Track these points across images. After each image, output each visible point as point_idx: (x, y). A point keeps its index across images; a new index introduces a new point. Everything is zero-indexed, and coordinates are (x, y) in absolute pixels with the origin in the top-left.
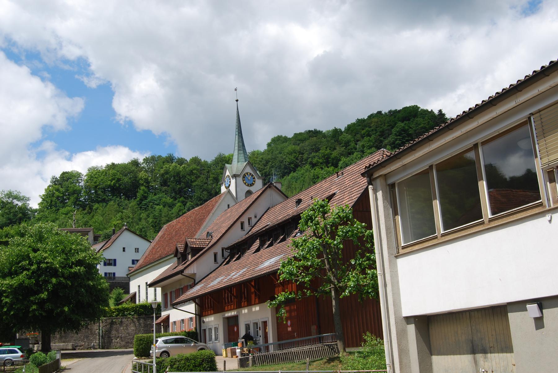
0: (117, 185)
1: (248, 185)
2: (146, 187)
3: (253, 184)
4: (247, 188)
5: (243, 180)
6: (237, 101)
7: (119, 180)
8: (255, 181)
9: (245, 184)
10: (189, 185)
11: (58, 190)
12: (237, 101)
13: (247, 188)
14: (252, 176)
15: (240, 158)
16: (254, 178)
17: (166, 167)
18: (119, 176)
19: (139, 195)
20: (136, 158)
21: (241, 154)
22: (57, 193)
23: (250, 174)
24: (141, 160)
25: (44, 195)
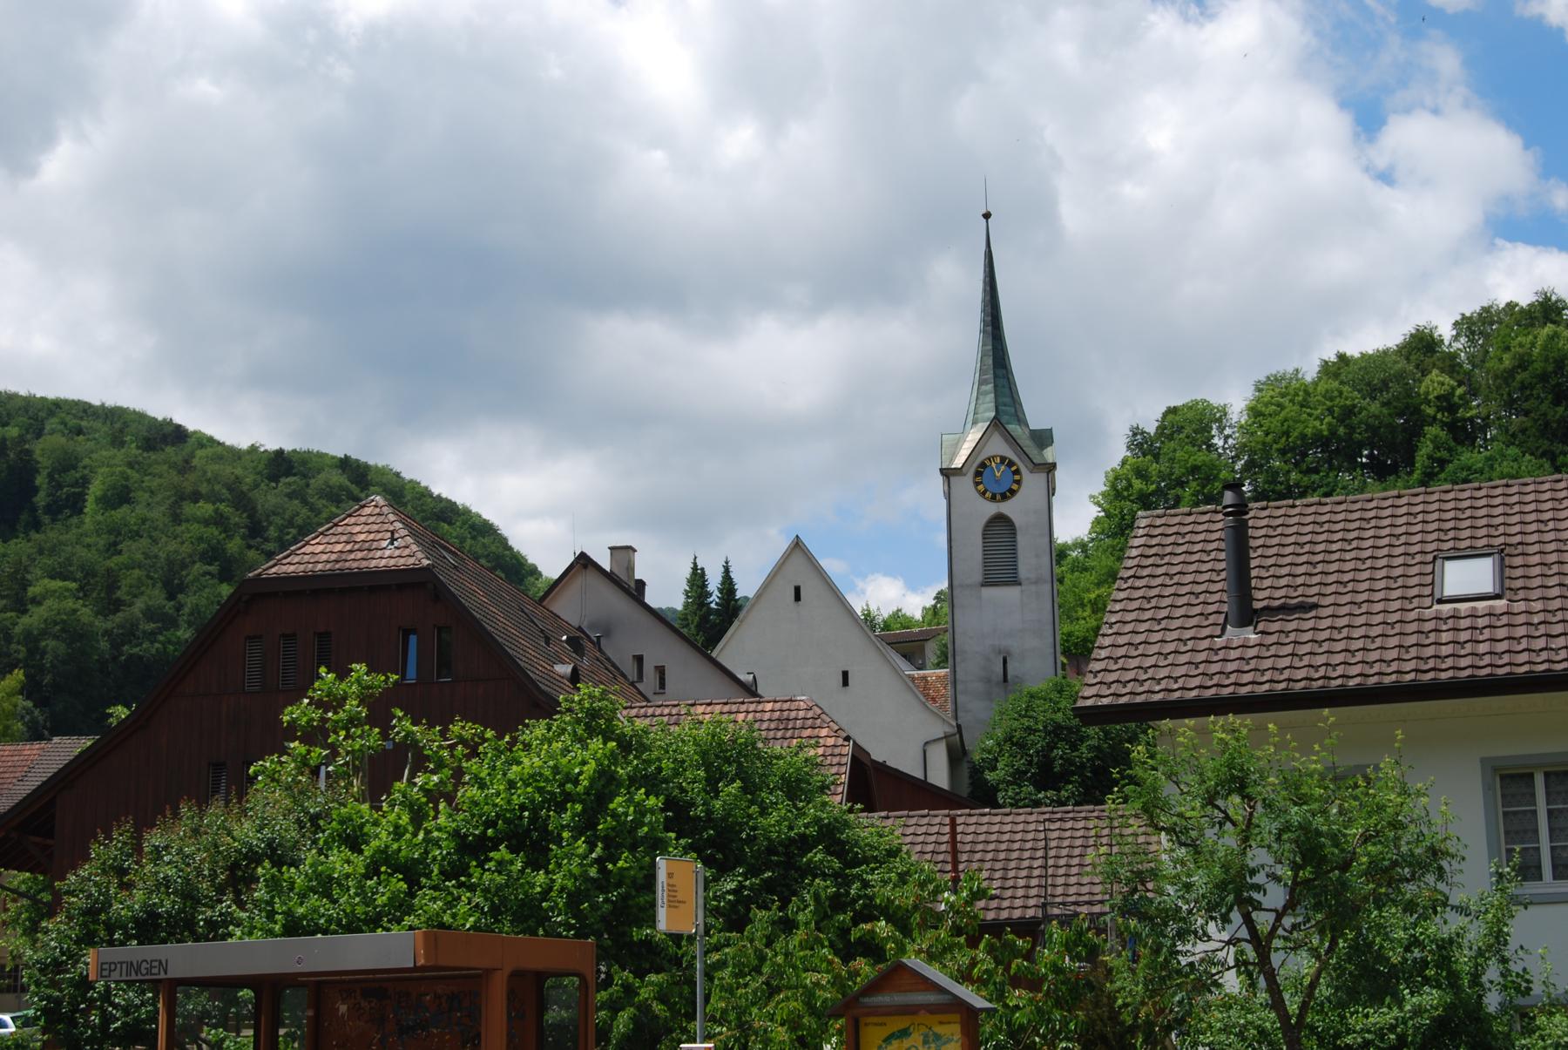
1: (993, 498)
3: (1013, 492)
4: (992, 509)
5: (977, 484)
6: (987, 216)
7: (1349, 412)
8: (1018, 482)
9: (983, 494)
11: (1141, 473)
12: (987, 216)
14: (1011, 463)
15: (981, 409)
16: (1017, 472)
17: (1521, 345)
18: (1352, 396)
21: (986, 393)
22: (1138, 484)
23: (1003, 459)
24: (1445, 331)
25: (1103, 494)
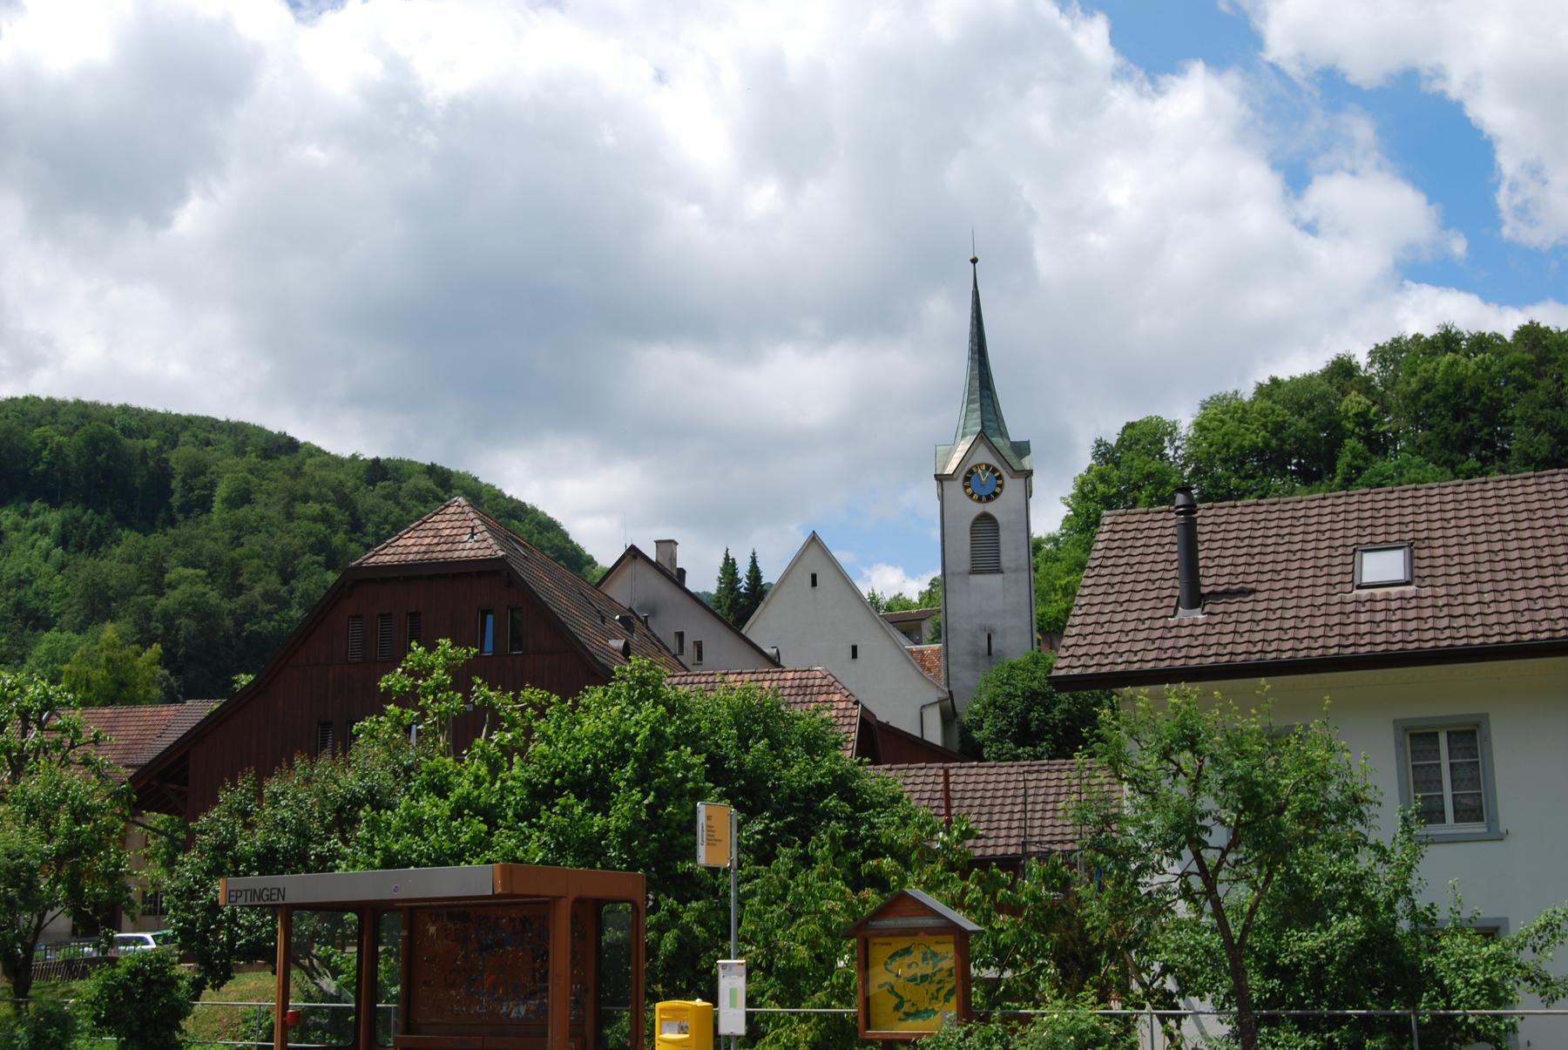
0: (1274, 442)
1: (980, 500)
2: (1360, 438)
3: (996, 495)
4: (978, 508)
5: (966, 488)
6: (974, 261)
7: (1279, 428)
8: (1001, 486)
10: (1493, 412)
11: (1103, 478)
12: (974, 261)
13: (978, 508)
14: (995, 470)
15: (969, 424)
16: (1000, 477)
17: (1426, 371)
18: (1282, 413)
19: (1341, 466)
20: (1341, 351)
21: (974, 411)
22: (1101, 488)
23: (988, 467)
24: (1362, 359)
